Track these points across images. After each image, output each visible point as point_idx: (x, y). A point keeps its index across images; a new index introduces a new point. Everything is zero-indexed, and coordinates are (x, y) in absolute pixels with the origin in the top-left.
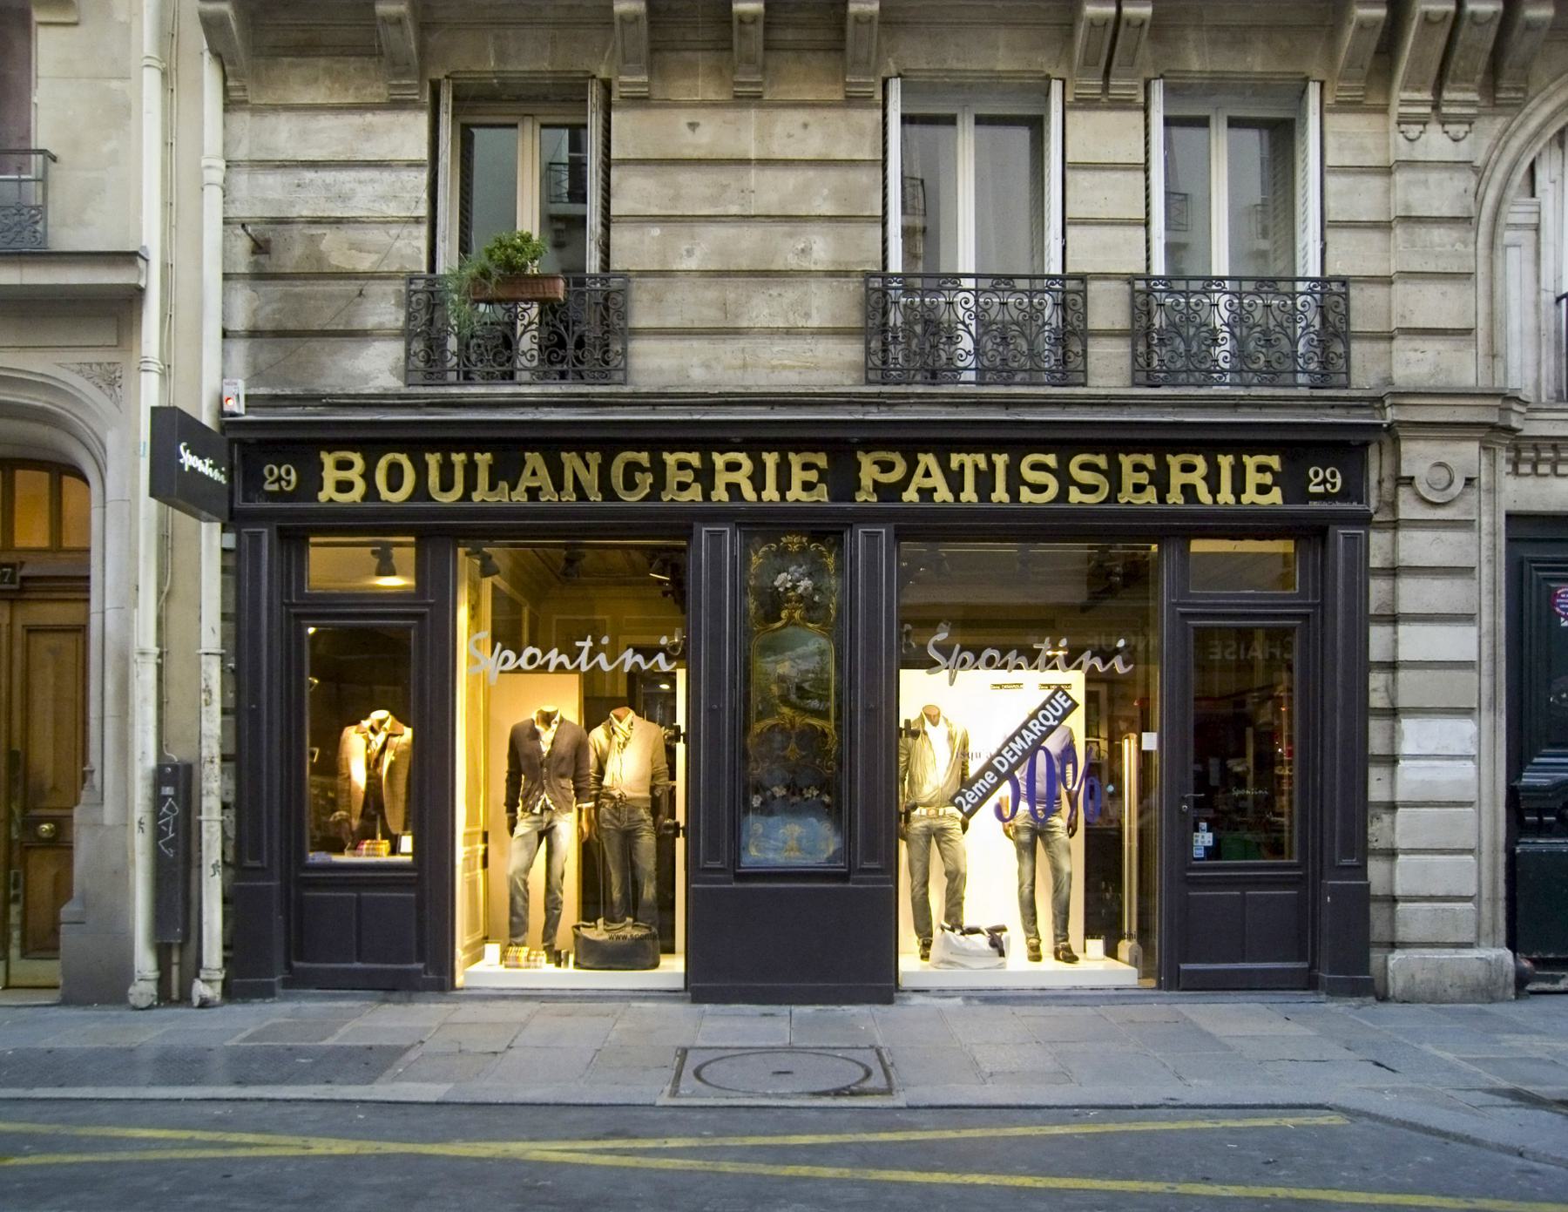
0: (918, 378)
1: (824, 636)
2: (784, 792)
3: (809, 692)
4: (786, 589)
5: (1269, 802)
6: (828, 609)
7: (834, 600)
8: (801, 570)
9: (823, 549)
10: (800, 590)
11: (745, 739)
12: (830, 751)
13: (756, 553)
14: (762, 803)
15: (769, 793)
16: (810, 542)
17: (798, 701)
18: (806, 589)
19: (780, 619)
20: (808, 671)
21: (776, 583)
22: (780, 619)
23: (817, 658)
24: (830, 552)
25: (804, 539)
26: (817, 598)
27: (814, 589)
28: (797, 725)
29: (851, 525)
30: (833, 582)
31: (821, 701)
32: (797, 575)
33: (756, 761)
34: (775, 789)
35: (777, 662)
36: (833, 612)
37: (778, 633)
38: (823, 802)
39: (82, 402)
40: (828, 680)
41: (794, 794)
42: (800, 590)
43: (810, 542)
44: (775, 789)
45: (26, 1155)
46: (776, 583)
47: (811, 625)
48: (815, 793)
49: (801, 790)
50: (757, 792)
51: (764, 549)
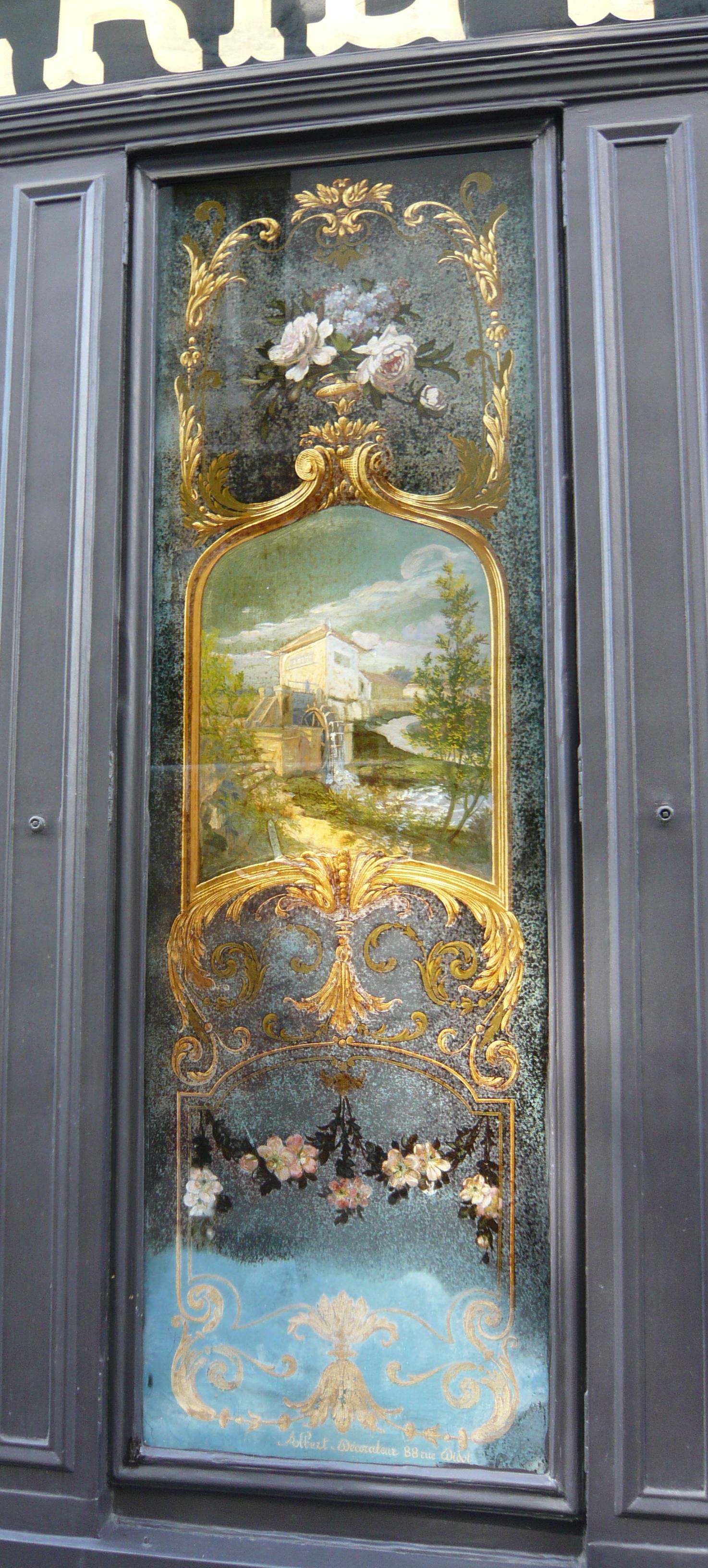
0: (292, 895)
1: (464, 537)
2: (308, 1161)
3: (402, 755)
4: (316, 371)
5: (544, 821)
6: (477, 433)
7: (499, 396)
8: (369, 299)
9: (451, 216)
10: (367, 372)
11: (157, 942)
12: (497, 994)
13: (205, 252)
14: (223, 1204)
15: (247, 1165)
16: (400, 199)
17: (364, 795)
18: (389, 365)
19: (294, 482)
20: (400, 676)
21: (276, 355)
22: (294, 482)
23: (439, 623)
24: (480, 227)
25: (381, 191)
26: (431, 398)
27: (420, 363)
28: (360, 890)
29: (555, 116)
30: (493, 334)
31: (454, 790)
32: (354, 318)
33: (197, 1029)
34: (273, 1148)
35: (280, 645)
36: (497, 445)
37: (278, 537)
38: (468, 1210)
39: (119, 708)
40: (482, 709)
41: (345, 1170)
42: (367, 372)
43: (400, 199)
44: (273, 1148)
45: (180, 883)
46: (276, 355)
47: (410, 499)
48: (437, 1168)
49: (377, 1156)
50: (202, 1160)
51: (234, 238)
